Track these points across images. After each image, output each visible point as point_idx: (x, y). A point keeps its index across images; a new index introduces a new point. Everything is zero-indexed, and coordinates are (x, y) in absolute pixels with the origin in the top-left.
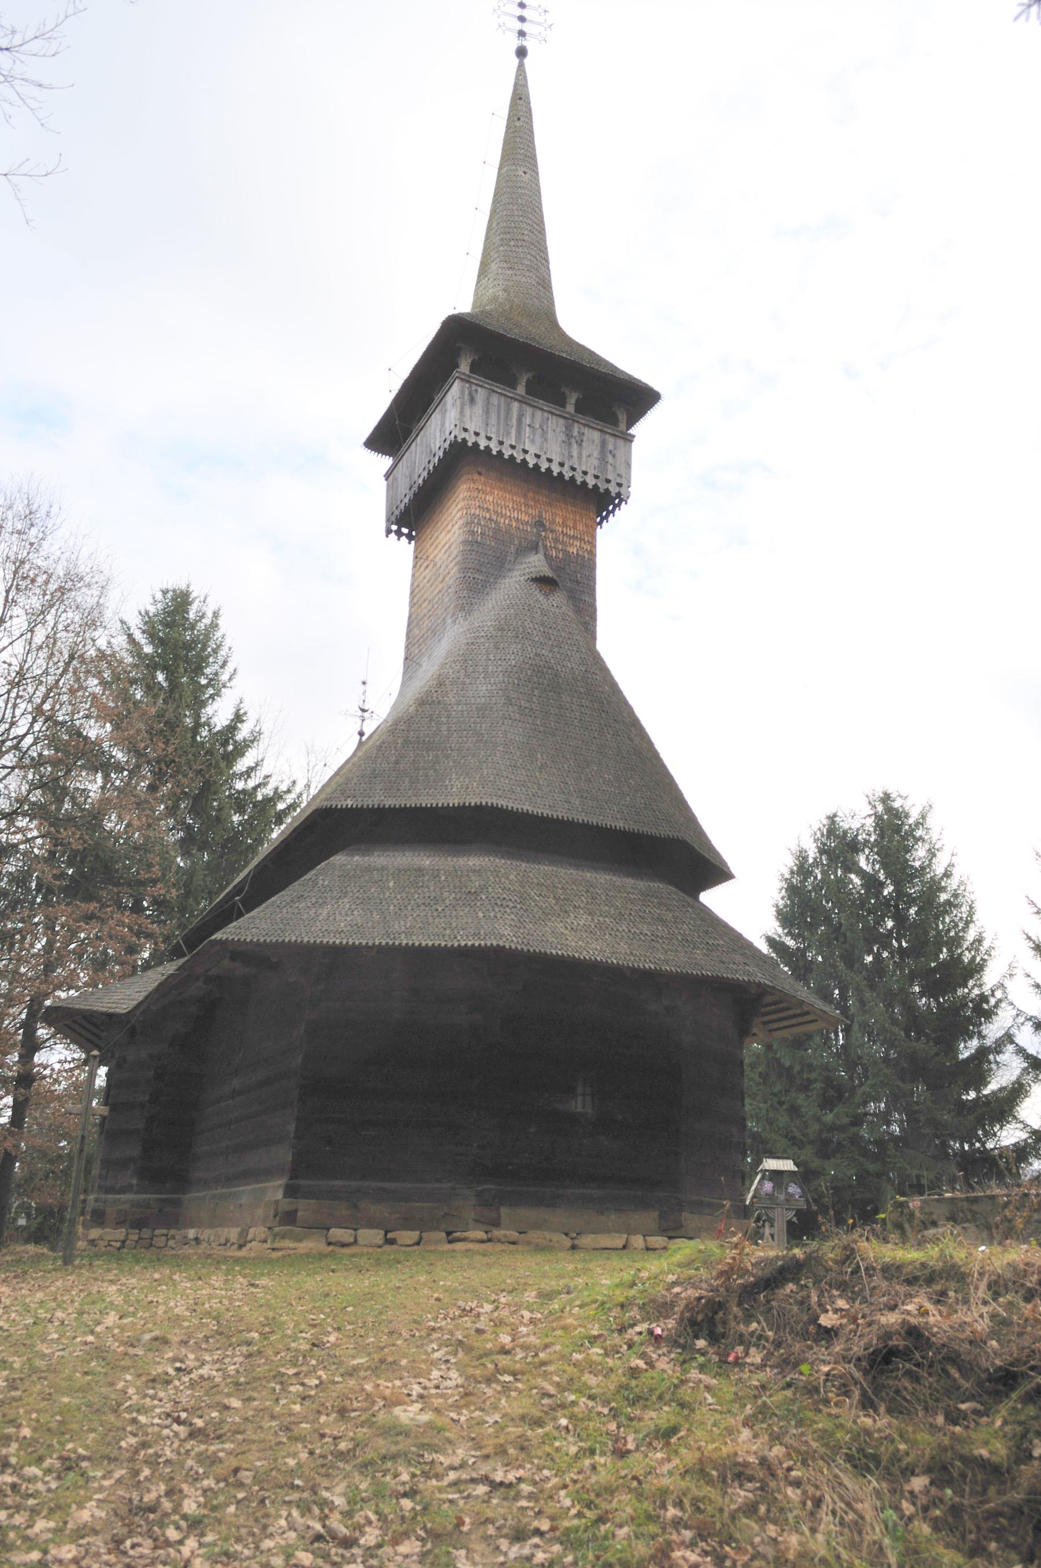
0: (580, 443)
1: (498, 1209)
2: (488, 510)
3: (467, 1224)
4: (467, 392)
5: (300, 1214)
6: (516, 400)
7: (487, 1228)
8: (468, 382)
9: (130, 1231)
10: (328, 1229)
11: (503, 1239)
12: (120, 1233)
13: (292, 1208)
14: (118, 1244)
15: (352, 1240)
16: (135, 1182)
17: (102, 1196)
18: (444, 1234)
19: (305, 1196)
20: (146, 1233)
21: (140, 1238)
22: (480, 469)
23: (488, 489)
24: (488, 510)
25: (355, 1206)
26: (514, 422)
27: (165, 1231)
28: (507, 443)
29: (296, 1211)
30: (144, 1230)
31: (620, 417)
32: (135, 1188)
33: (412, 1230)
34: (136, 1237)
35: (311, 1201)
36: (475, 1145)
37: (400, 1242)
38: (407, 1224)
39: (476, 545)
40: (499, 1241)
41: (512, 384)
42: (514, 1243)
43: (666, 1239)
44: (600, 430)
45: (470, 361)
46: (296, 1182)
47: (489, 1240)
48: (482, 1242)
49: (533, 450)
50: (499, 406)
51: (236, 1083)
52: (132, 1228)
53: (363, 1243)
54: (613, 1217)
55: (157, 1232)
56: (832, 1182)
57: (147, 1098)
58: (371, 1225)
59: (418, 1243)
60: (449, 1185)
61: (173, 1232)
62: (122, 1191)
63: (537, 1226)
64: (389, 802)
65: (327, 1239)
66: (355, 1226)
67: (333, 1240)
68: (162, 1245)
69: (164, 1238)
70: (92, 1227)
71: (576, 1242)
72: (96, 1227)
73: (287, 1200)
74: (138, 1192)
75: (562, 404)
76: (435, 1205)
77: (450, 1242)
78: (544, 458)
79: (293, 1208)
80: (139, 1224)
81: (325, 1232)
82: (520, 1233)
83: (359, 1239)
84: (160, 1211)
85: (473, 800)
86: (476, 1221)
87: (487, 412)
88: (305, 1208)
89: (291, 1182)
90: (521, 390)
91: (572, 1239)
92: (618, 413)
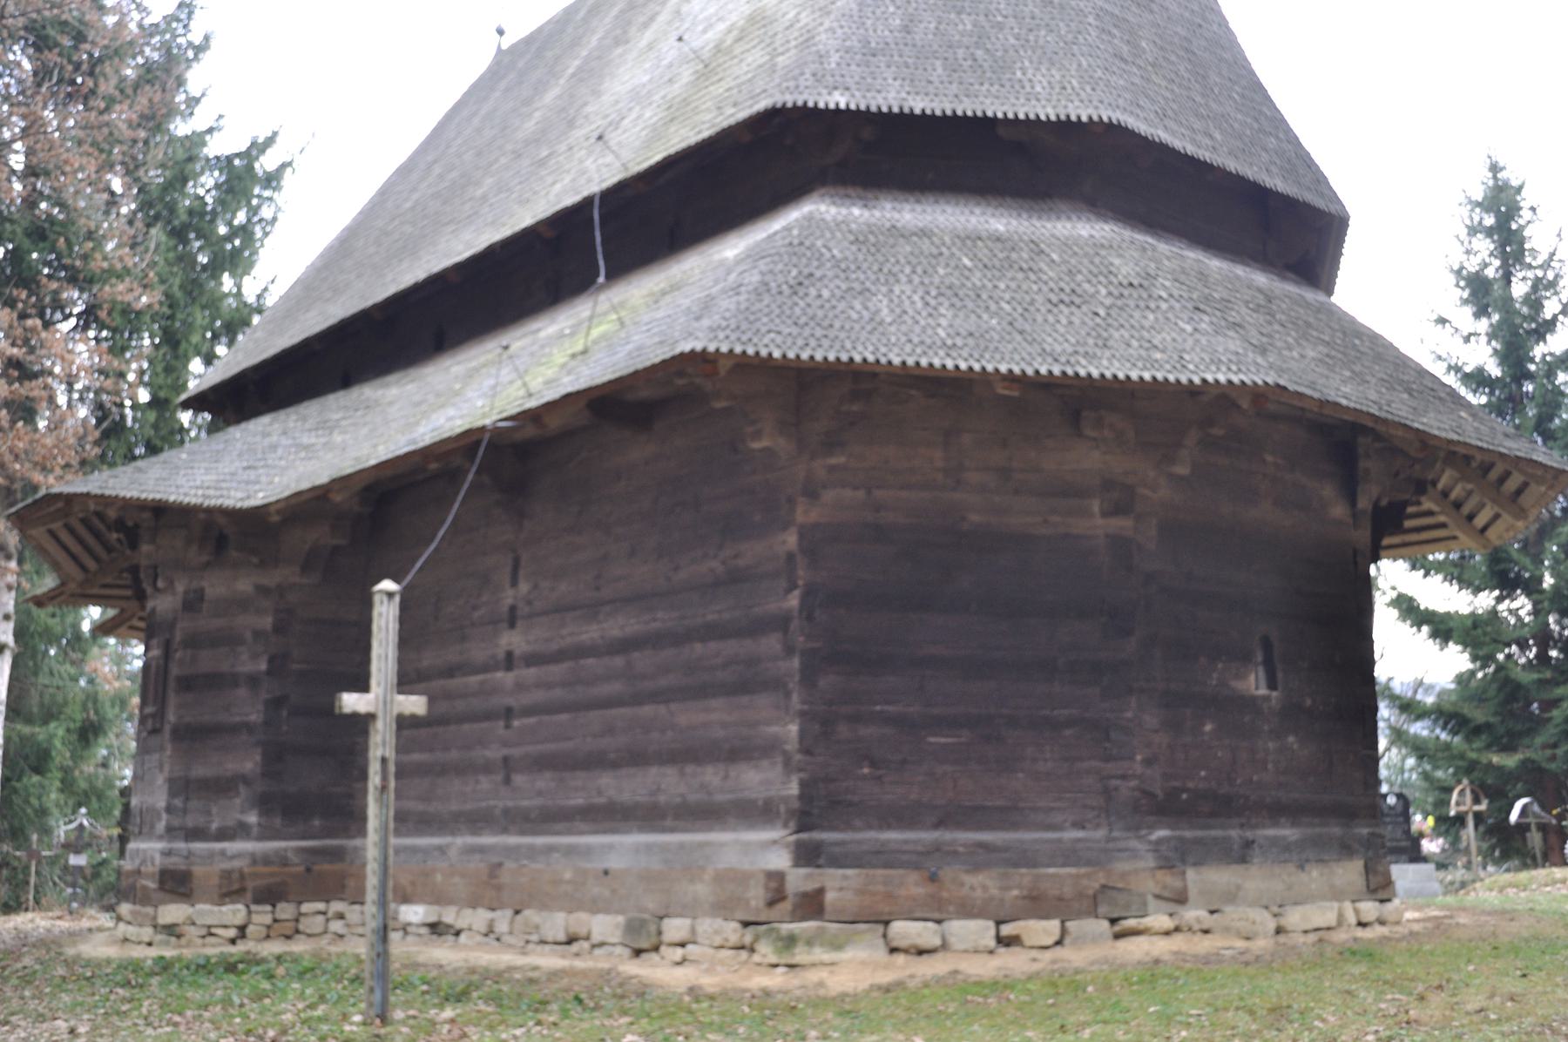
1: (1184, 873)
3: (1145, 904)
5: (830, 897)
7: (1172, 907)
9: (254, 907)
10: (887, 923)
11: (1196, 927)
12: (234, 912)
13: (810, 886)
14: (232, 933)
15: (937, 942)
16: (252, 819)
17: (180, 845)
18: (1105, 924)
19: (836, 862)
20: (286, 910)
21: (275, 921)
25: (933, 878)
27: (321, 906)
29: (821, 892)
30: (281, 906)
32: (255, 830)
33: (1046, 917)
34: (268, 919)
35: (850, 872)
36: (1139, 758)
37: (1027, 941)
38: (1037, 905)
40: (1190, 929)
42: (1206, 932)
43: (1377, 904)
46: (817, 835)
47: (1177, 929)
48: (1167, 933)
51: (514, 640)
52: (257, 901)
53: (962, 947)
54: (1315, 874)
55: (307, 907)
56: (1401, 786)
57: (263, 666)
58: (967, 911)
59: (1059, 943)
60: (1100, 833)
61: (337, 906)
62: (223, 835)
64: (918, 105)
65: (887, 944)
66: (937, 916)
67: (902, 944)
68: (319, 929)
69: (321, 918)
70: (164, 902)
71: (1283, 922)
72: (172, 901)
73: (803, 871)
74: (261, 838)
76: (1083, 870)
77: (1118, 936)
79: (817, 885)
80: (270, 895)
81: (880, 928)
82: (1212, 912)
83: (952, 940)
84: (308, 870)
85: (1081, 111)
86: (1158, 897)
88: (839, 884)
89: (804, 836)
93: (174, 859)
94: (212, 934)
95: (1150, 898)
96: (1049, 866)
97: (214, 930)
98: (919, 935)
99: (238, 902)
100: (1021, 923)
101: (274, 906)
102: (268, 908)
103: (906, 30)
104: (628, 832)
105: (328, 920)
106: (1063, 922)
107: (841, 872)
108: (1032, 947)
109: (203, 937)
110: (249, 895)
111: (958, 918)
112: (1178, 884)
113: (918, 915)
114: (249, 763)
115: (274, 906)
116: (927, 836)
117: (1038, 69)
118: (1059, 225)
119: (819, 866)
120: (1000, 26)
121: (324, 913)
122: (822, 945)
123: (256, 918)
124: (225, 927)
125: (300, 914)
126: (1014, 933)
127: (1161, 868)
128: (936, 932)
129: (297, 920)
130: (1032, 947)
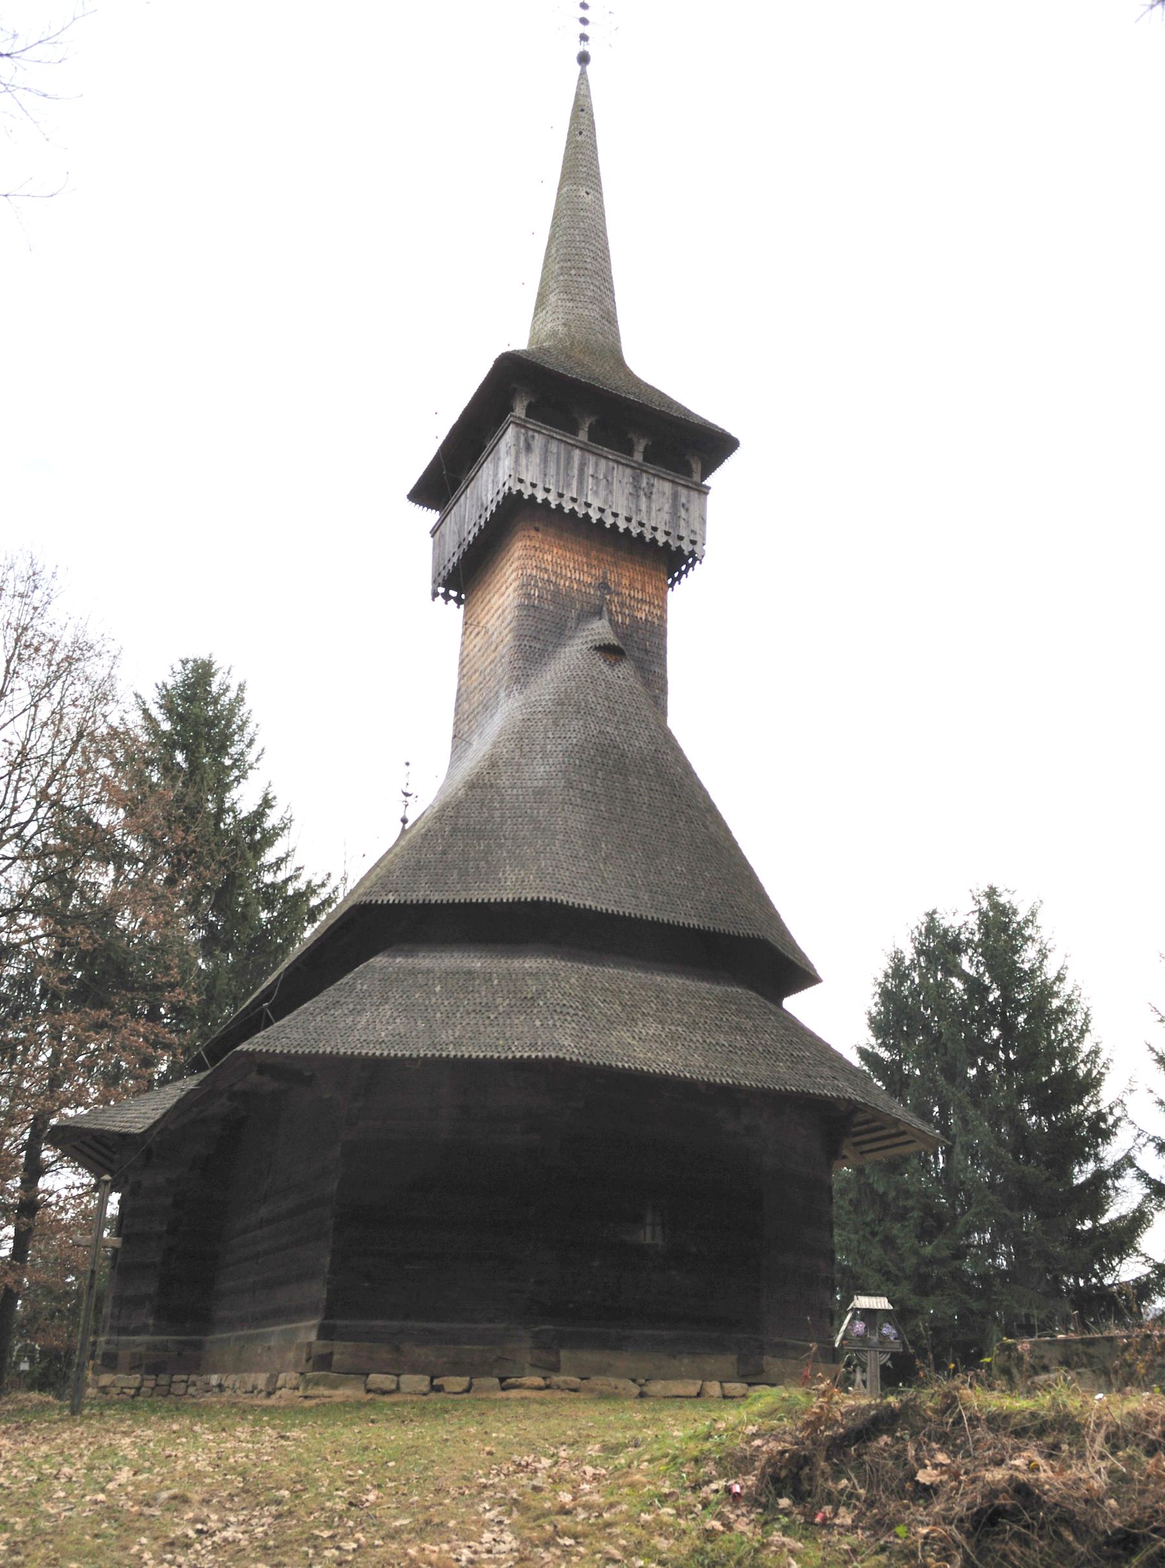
0: (649, 496)
1: (557, 1353)
2: (546, 570)
4: (522, 438)
5: (336, 1357)
6: (577, 447)
7: (545, 1373)
8: (524, 427)
9: (145, 1376)
10: (367, 1375)
11: (563, 1386)
12: (134, 1379)
13: (326, 1351)
14: (132, 1392)
15: (393, 1386)
17: (115, 1338)
19: (342, 1338)
20: (164, 1379)
21: (157, 1385)
22: (537, 525)
23: (547, 547)
24: (546, 570)
25: (397, 1349)
26: (576, 472)
27: (184, 1377)
28: (568, 495)
29: (331, 1354)
30: (162, 1376)
31: (694, 466)
32: (151, 1329)
34: (152, 1384)
36: (532, 1280)
37: (447, 1389)
38: (456, 1369)
39: (532, 610)
41: (574, 431)
43: (745, 1385)
44: (673, 482)
45: (526, 403)
47: (548, 1387)
48: (540, 1388)
49: (596, 503)
50: (558, 454)
52: (148, 1373)
53: (408, 1390)
54: (686, 1361)
55: (176, 1378)
56: (931, 1322)
58: (415, 1371)
61: (193, 1378)
62: (136, 1332)
63: (602, 1371)
66: (397, 1372)
67: (373, 1387)
69: (183, 1385)
70: (103, 1373)
71: (645, 1389)
72: (107, 1372)
73: (321, 1342)
75: (629, 452)
76: (487, 1348)
77: (503, 1389)
78: (608, 512)
79: (328, 1351)
80: (155, 1369)
82: (582, 1379)
83: (402, 1386)
84: (179, 1354)
85: (529, 895)
86: (533, 1365)
87: (545, 461)
88: (341, 1351)
90: (583, 436)
91: (641, 1385)
92: (692, 461)
93: (110, 1347)
94: (124, 1393)
95: (527, 1365)
96: (468, 1344)
97: (125, 1390)
98: (382, 1382)
99: (137, 1373)
100: (445, 1378)
101: (157, 1376)
102: (154, 1377)
103: (444, 853)
104: (278, 1324)
105: (188, 1387)
106: (471, 1378)
107: (344, 1343)
108: (449, 1393)
109: (118, 1394)
110: (143, 1368)
111: (408, 1374)
112: (553, 1359)
113: (385, 1370)
114: (151, 1288)
115: (157, 1376)
116: (396, 1324)
117: (513, 871)
118: (516, 962)
119: (331, 1340)
120: (501, 846)
121: (187, 1382)
122: (324, 1386)
123: (146, 1383)
124: (130, 1388)
125: (172, 1382)
126: (440, 1383)
127: (539, 1348)
128: (393, 1380)
129: (170, 1386)
130: (449, 1393)
